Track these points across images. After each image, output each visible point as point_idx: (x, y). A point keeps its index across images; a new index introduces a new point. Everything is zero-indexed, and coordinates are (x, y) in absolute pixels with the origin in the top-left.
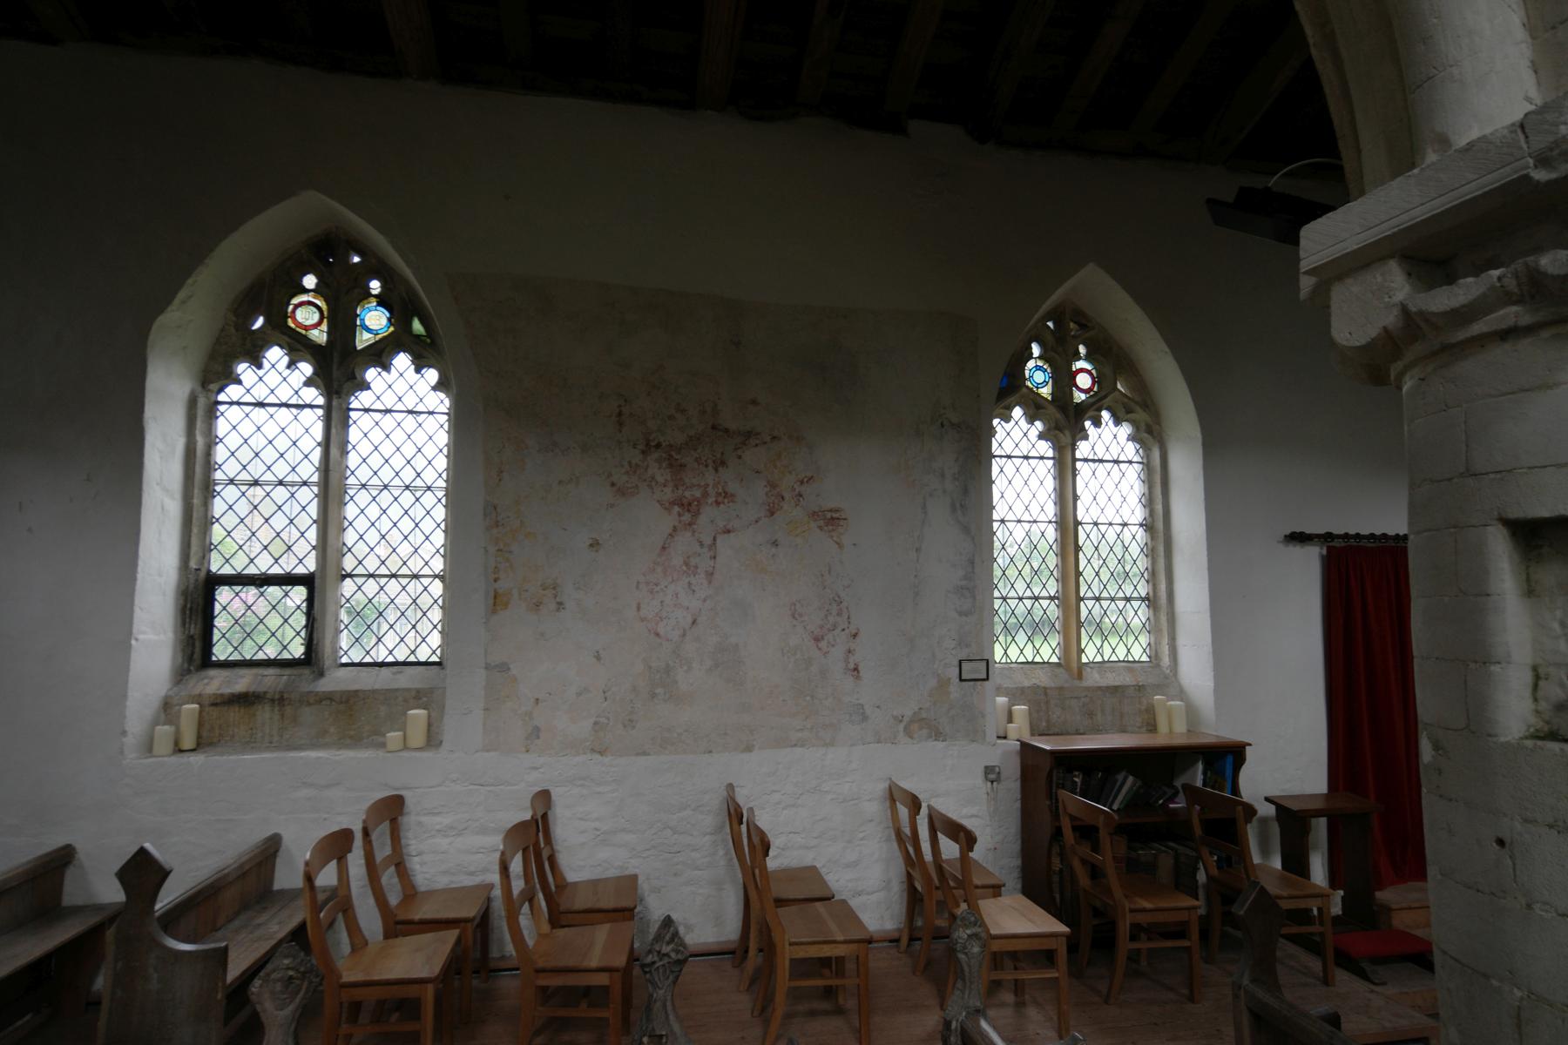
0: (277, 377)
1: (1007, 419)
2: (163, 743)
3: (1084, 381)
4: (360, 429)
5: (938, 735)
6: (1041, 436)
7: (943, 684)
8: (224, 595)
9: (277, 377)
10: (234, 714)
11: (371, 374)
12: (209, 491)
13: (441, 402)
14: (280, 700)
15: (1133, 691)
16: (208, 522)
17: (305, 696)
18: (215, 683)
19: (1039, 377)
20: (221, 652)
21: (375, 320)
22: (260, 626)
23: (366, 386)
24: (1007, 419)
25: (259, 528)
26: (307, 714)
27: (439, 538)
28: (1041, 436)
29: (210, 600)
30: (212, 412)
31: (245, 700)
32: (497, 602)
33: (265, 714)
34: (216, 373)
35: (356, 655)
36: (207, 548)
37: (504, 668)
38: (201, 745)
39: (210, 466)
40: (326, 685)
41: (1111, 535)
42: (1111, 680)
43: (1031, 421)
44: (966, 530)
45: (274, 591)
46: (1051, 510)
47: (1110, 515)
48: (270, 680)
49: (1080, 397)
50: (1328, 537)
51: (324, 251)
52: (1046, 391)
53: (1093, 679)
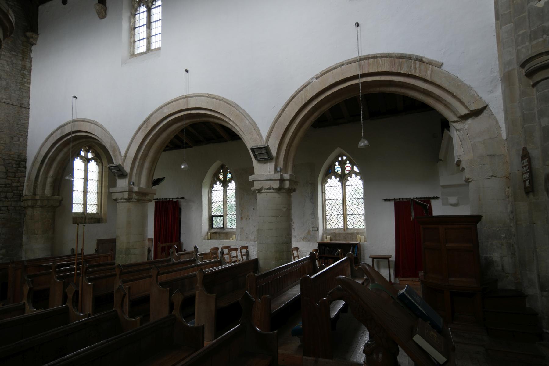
0: (218, 186)
1: (331, 179)
2: (206, 238)
3: (348, 169)
4: (348, 189)
5: (308, 241)
6: (339, 181)
7: (309, 232)
8: (214, 218)
9: (218, 186)
10: (214, 235)
11: (349, 178)
12: (325, 200)
13: (361, 182)
14: (219, 233)
15: (354, 233)
16: (212, 208)
17: (222, 233)
18: (213, 231)
19: (338, 169)
20: (214, 226)
21: (229, 175)
22: (218, 223)
23: (348, 181)
24: (331, 179)
25: (217, 209)
26: (222, 235)
27: (363, 206)
28: (339, 181)
29: (212, 219)
30: (211, 192)
31: (215, 233)
32: (242, 218)
33: (218, 235)
34: (324, 181)
35: (229, 227)
36: (212, 212)
37: (242, 228)
38: (211, 239)
39: (211, 200)
40: (224, 231)
41: (334, 202)
42: (352, 231)
43: (336, 178)
44: (313, 203)
45: (219, 218)
46: (341, 197)
47: (334, 197)
48: (219, 230)
49: (347, 172)
50: (394, 199)
51: (222, 167)
52: (222, 179)
53: (349, 231)
